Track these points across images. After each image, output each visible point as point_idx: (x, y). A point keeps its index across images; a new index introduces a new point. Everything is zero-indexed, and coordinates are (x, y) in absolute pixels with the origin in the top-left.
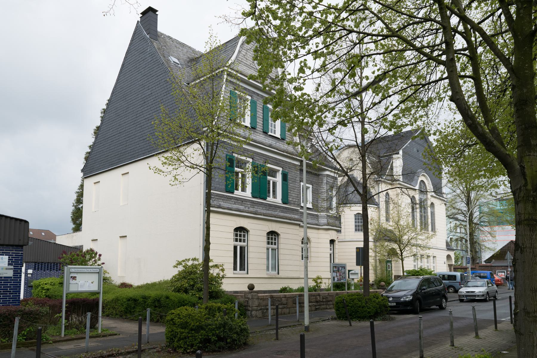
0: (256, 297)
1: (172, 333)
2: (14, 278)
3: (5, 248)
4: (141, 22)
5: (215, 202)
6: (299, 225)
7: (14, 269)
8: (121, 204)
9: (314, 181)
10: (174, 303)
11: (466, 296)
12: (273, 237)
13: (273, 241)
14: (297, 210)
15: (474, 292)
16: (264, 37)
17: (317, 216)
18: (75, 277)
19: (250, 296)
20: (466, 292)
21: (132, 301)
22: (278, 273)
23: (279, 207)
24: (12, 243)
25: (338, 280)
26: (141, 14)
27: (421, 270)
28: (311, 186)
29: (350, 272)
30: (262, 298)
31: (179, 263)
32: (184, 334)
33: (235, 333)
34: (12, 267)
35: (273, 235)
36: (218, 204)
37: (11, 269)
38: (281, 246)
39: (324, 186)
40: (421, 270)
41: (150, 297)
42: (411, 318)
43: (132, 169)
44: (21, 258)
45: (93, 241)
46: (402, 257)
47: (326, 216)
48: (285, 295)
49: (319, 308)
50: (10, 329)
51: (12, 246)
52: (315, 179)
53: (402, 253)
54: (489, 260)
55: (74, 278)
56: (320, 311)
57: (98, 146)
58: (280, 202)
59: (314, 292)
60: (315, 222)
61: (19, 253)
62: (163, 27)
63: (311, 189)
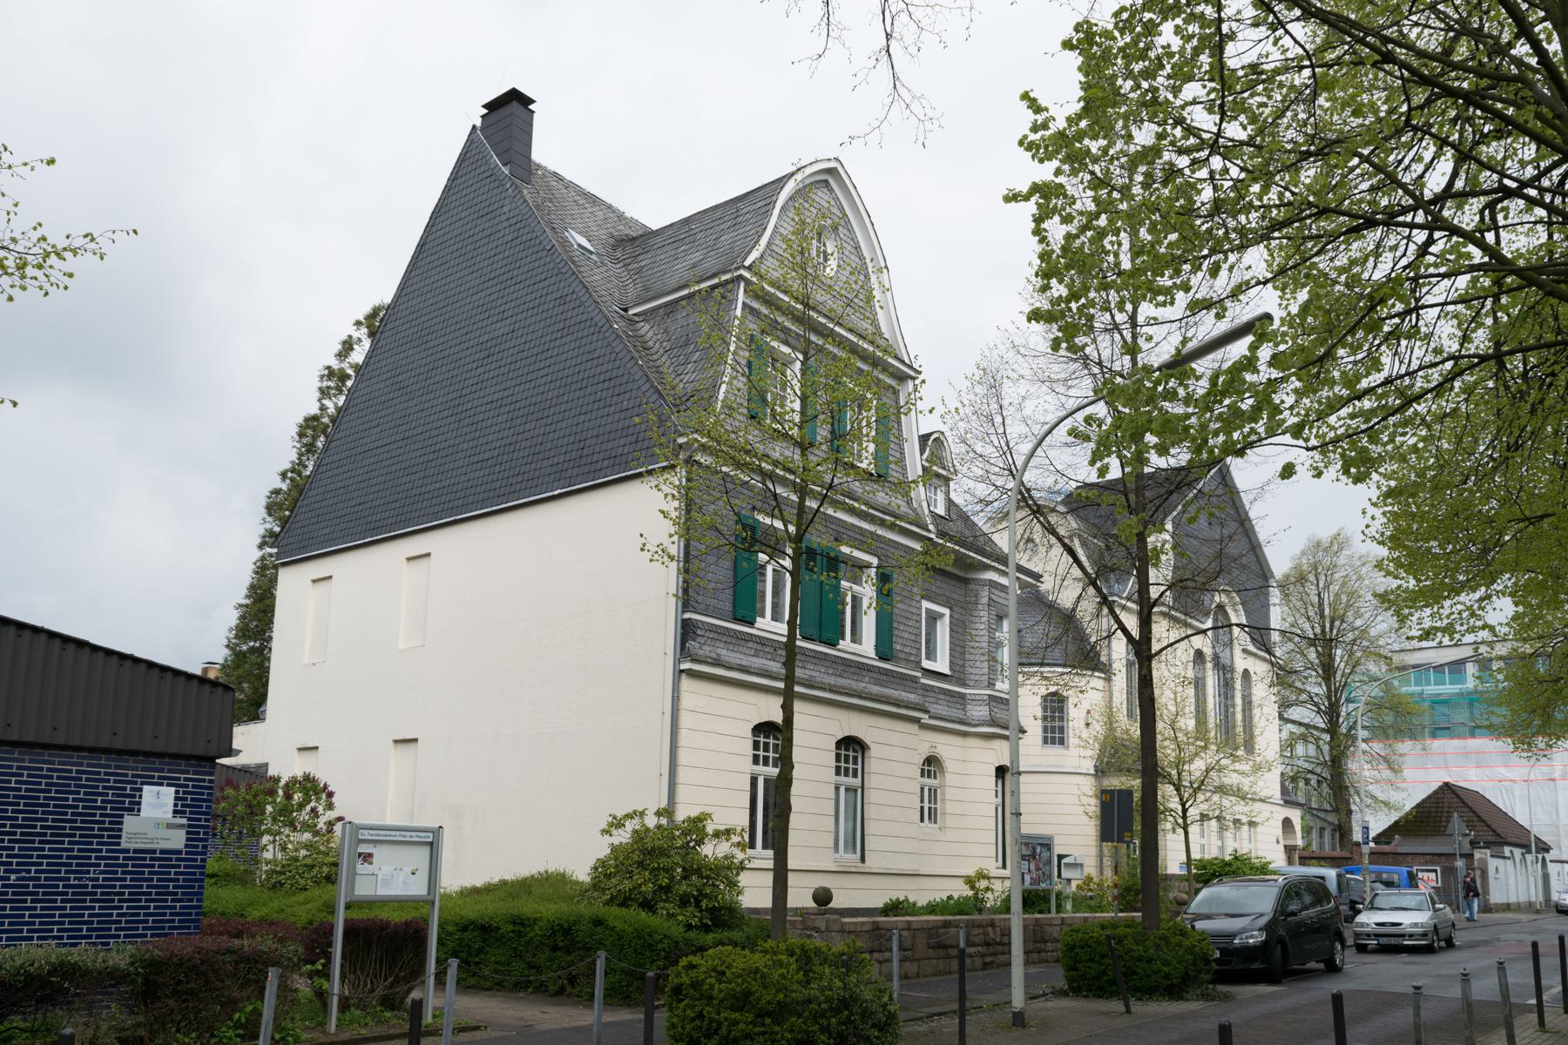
0: (837, 927)
1: (698, 1023)
2: (187, 853)
3: (168, 764)
4: (483, 128)
5: (705, 647)
6: (917, 721)
7: (189, 826)
8: (402, 645)
9: (955, 596)
10: (619, 939)
11: (1377, 936)
12: (851, 754)
13: (851, 766)
14: (914, 679)
15: (1400, 924)
16: (1205, 252)
17: (962, 696)
18: (370, 855)
19: (820, 923)
20: (1377, 924)
21: (473, 930)
22: (863, 860)
23: (869, 669)
24: (187, 751)
25: (1035, 882)
26: (485, 106)
27: (1236, 858)
28: (946, 611)
29: (1064, 861)
30: (852, 929)
31: (617, 823)
32: (742, 1026)
33: (874, 1026)
34: (184, 821)
35: (851, 747)
36: (714, 655)
37: (181, 826)
38: (872, 781)
39: (982, 613)
40: (1236, 858)
41: (536, 920)
42: (1272, 996)
43: (437, 543)
44: (209, 794)
45: (303, 753)
46: (1185, 822)
47: (986, 698)
48: (909, 922)
49: (992, 962)
50: (201, 1006)
51: (187, 757)
52: (956, 592)
53: (1185, 811)
54: (1386, 836)
55: (367, 858)
56: (995, 971)
57: (330, 474)
58: (871, 652)
59: (976, 917)
60: (956, 713)
61: (204, 781)
62: (548, 149)
63: (947, 619)
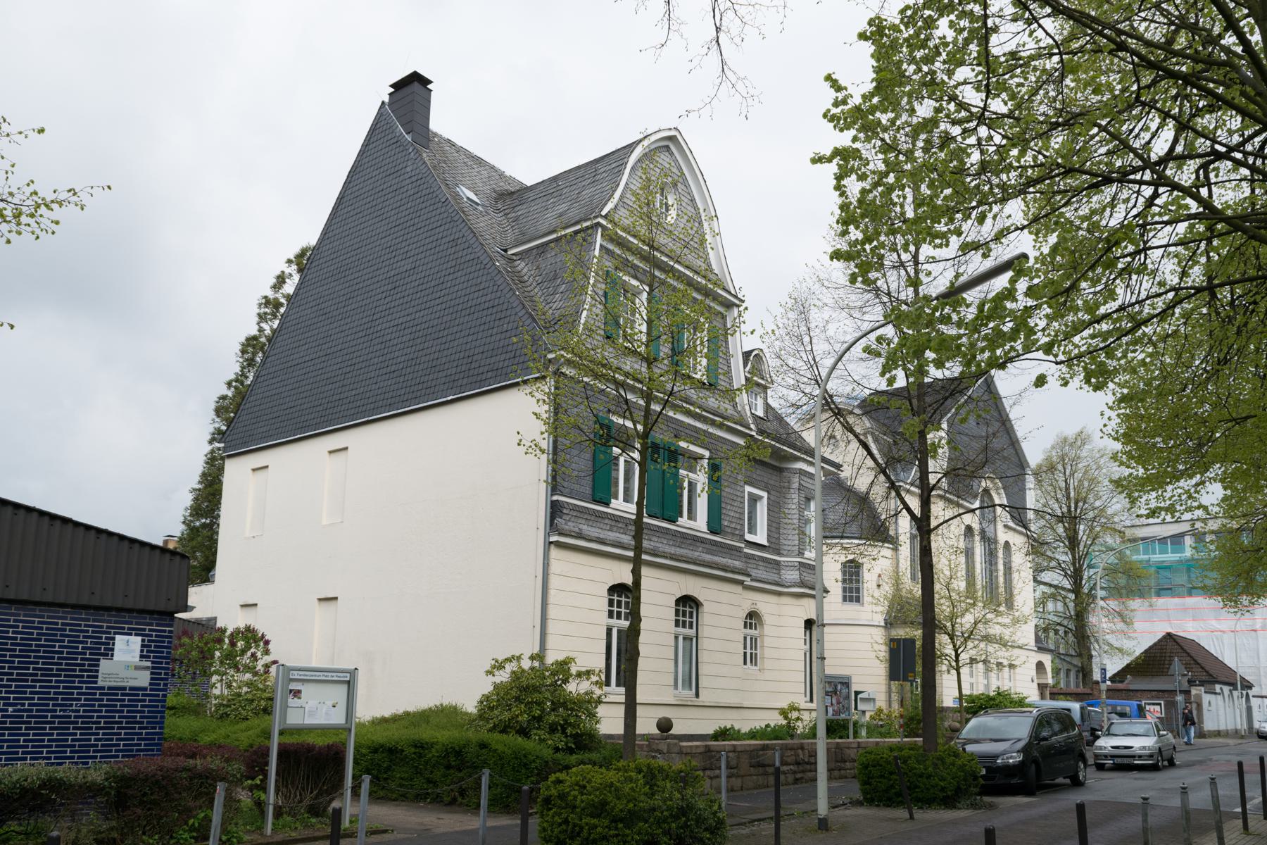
0: (676, 749)
1: (564, 827)
2: (151, 690)
3: (135, 618)
4: (390, 104)
5: (570, 524)
6: (741, 583)
7: (153, 668)
8: (325, 522)
9: (772, 482)
10: (501, 759)
11: (1113, 757)
12: (688, 609)
13: (688, 619)
14: (738, 549)
15: (1131, 747)
16: (974, 204)
17: (777, 563)
18: (299, 691)
19: (663, 746)
20: (1112, 747)
21: (382, 752)
22: (697, 695)
23: (702, 541)
24: (151, 607)
25: (836, 713)
26: (392, 86)
27: (999, 694)
28: (765, 494)
29: (860, 696)
30: (689, 751)
31: (499, 666)
32: (599, 830)
33: (706, 829)
34: (149, 664)
35: (687, 604)
36: (577, 530)
37: (147, 668)
38: (705, 632)
39: (793, 496)
40: (999, 694)
41: (433, 744)
42: (1028, 805)
43: (353, 439)
44: (169, 642)
45: (245, 609)
46: (957, 664)
47: (796, 564)
48: (734, 746)
49: (802, 778)
50: (162, 814)
51: (151, 612)
52: (773, 479)
53: (957, 656)
54: (1120, 676)
55: (297, 693)
56: (804, 785)
57: (267, 383)
58: (704, 528)
59: (789, 741)
60: (772, 577)
61: (165, 631)
62: (442, 120)
63: (765, 500)
